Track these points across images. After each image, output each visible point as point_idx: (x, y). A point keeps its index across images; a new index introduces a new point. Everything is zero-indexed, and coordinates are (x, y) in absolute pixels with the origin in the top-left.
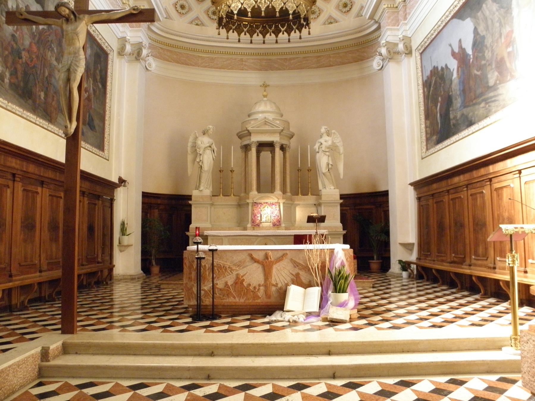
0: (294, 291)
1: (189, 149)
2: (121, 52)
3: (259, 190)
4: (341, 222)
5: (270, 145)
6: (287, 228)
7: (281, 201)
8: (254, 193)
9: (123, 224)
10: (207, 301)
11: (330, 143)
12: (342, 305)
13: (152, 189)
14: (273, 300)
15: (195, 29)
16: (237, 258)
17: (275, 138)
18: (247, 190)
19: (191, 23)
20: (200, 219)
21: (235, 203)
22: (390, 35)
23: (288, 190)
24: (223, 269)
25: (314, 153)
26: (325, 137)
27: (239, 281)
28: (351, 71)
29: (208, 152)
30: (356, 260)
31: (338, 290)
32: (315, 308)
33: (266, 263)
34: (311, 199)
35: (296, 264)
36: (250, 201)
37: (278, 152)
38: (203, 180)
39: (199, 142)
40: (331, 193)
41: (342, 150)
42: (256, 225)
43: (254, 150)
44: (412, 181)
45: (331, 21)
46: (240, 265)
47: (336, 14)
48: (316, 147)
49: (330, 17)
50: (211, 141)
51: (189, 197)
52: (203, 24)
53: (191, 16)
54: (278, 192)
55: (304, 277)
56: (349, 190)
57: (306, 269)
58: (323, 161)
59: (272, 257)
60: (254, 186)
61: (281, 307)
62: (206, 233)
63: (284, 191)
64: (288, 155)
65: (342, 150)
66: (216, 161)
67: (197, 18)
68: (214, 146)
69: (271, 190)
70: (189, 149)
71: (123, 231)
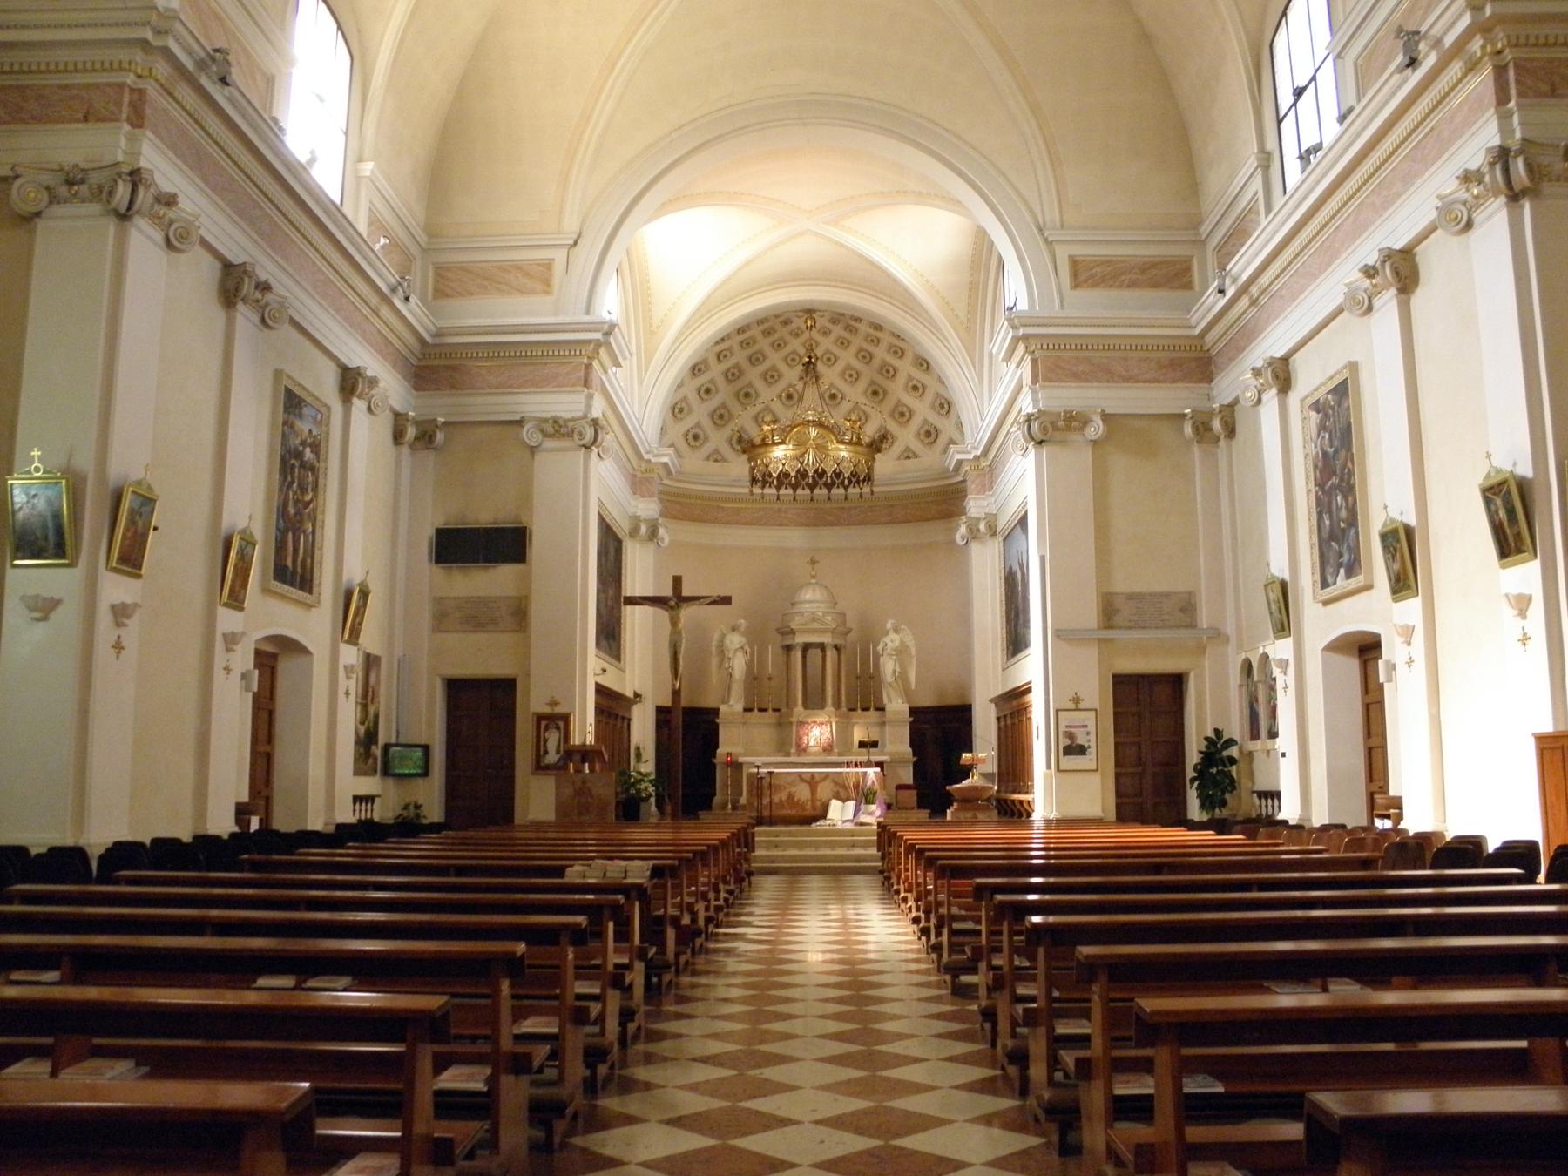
0: (835, 805)
1: (713, 649)
2: (634, 534)
3: (806, 706)
4: (912, 745)
5: (822, 647)
6: (840, 754)
7: (834, 721)
8: (799, 709)
9: (638, 749)
10: (766, 813)
11: (897, 644)
12: (871, 814)
13: (661, 703)
14: (818, 812)
15: (714, 467)
16: (789, 779)
17: (827, 639)
18: (790, 704)
19: (708, 458)
20: (730, 743)
21: (773, 721)
22: (976, 506)
23: (844, 704)
24: (779, 788)
25: (877, 657)
26: (892, 636)
27: (791, 797)
28: (932, 532)
29: (740, 655)
30: (1395, 979)
31: (869, 802)
32: (850, 817)
33: (812, 782)
34: (873, 715)
35: (836, 783)
36: (794, 720)
37: (830, 653)
38: (733, 693)
39: (727, 642)
40: (898, 706)
41: (913, 651)
42: (802, 750)
43: (798, 654)
44: (993, 695)
45: (909, 454)
46: (792, 784)
47: (916, 446)
48: (880, 648)
49: (908, 449)
50: (744, 640)
51: (716, 712)
52: (724, 460)
53: (708, 448)
54: (830, 708)
55: (843, 794)
56: (927, 700)
57: (844, 787)
58: (888, 667)
59: (817, 778)
60: (800, 702)
61: (824, 816)
62: (741, 760)
63: (837, 705)
64: (843, 658)
65: (913, 651)
66: (749, 666)
67: (716, 451)
68: (747, 648)
69: (821, 706)
70: (713, 649)
71: (638, 755)
